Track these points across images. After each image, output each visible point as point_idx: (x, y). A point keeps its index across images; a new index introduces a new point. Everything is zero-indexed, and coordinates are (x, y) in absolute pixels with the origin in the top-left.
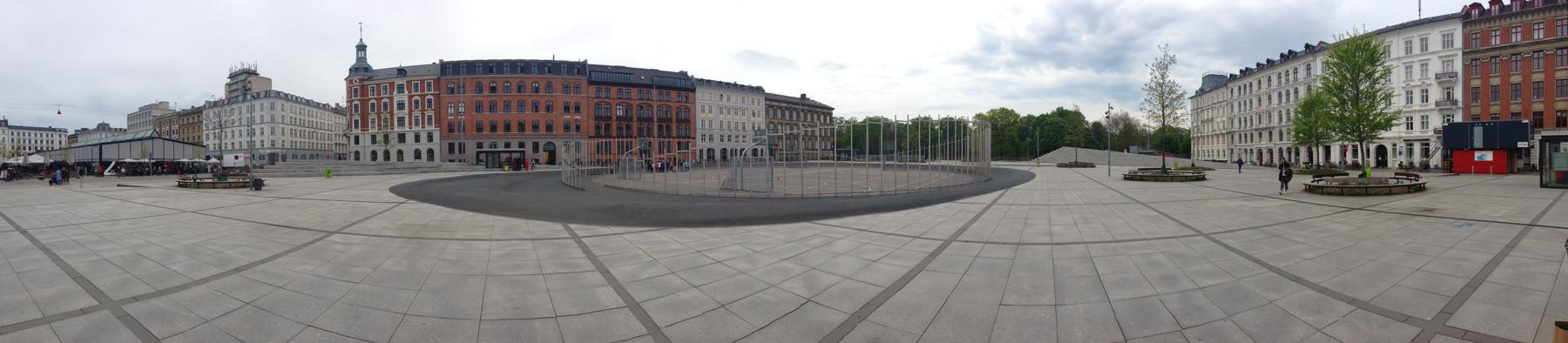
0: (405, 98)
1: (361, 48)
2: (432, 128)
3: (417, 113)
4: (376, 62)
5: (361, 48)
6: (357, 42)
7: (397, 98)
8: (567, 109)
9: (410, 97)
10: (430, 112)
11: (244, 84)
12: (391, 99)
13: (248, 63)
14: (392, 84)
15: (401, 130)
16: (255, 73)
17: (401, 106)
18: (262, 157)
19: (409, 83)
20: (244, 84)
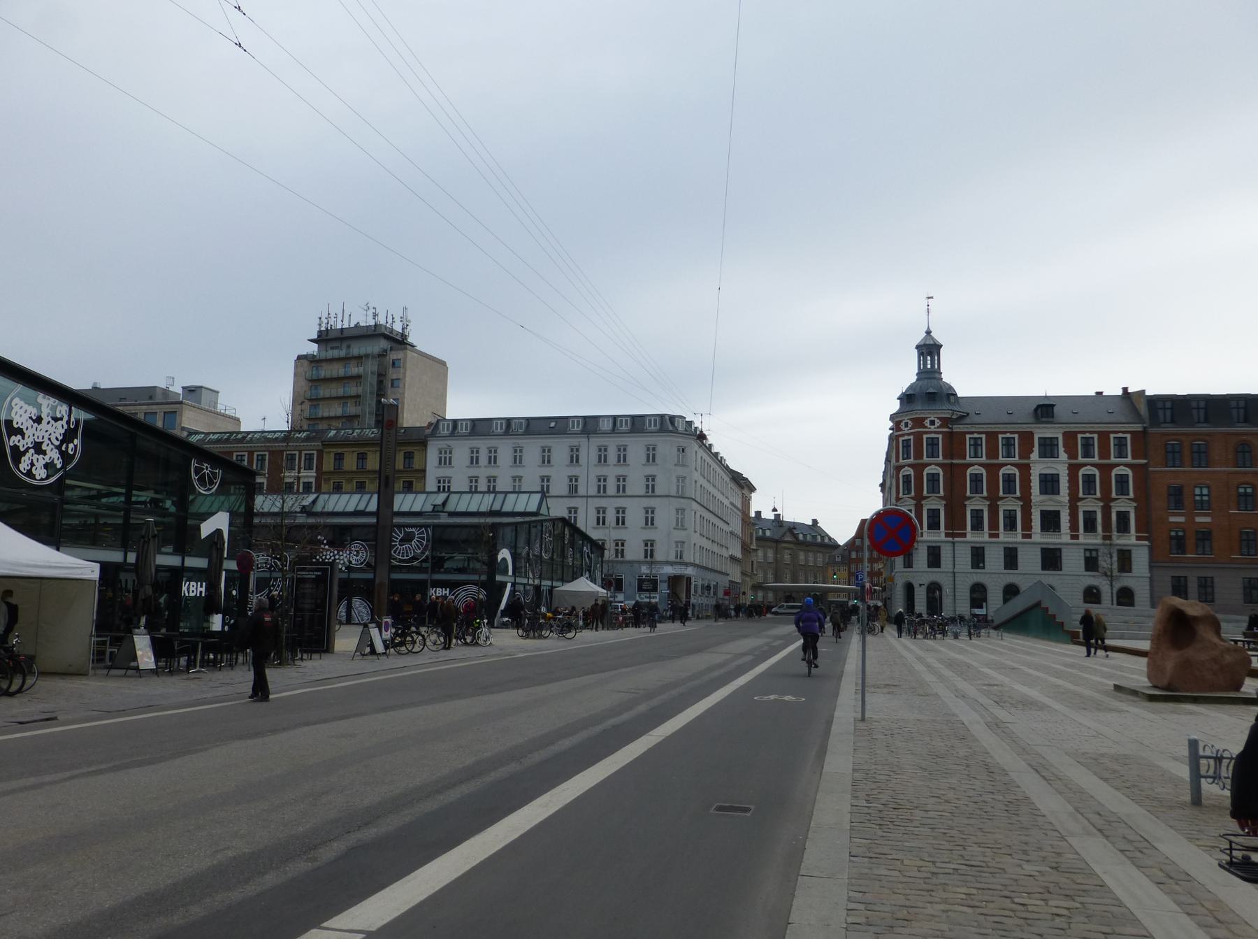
0: (1059, 466)
1: (929, 350)
2: (1130, 539)
3: (1091, 504)
4: (968, 378)
5: (929, 350)
6: (919, 337)
7: (1039, 466)
8: (1204, 536)
9: (1073, 469)
10: (1124, 504)
11: (358, 370)
12: (1025, 469)
13: (389, 313)
14: (1027, 437)
15: (1051, 540)
16: (400, 342)
17: (1050, 484)
18: (647, 585)
19: (1070, 437)
20: (358, 370)
